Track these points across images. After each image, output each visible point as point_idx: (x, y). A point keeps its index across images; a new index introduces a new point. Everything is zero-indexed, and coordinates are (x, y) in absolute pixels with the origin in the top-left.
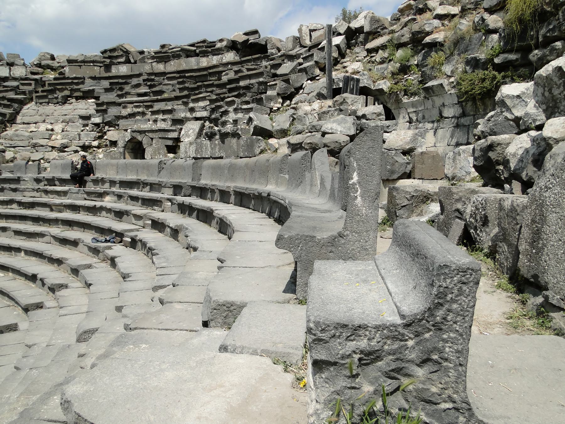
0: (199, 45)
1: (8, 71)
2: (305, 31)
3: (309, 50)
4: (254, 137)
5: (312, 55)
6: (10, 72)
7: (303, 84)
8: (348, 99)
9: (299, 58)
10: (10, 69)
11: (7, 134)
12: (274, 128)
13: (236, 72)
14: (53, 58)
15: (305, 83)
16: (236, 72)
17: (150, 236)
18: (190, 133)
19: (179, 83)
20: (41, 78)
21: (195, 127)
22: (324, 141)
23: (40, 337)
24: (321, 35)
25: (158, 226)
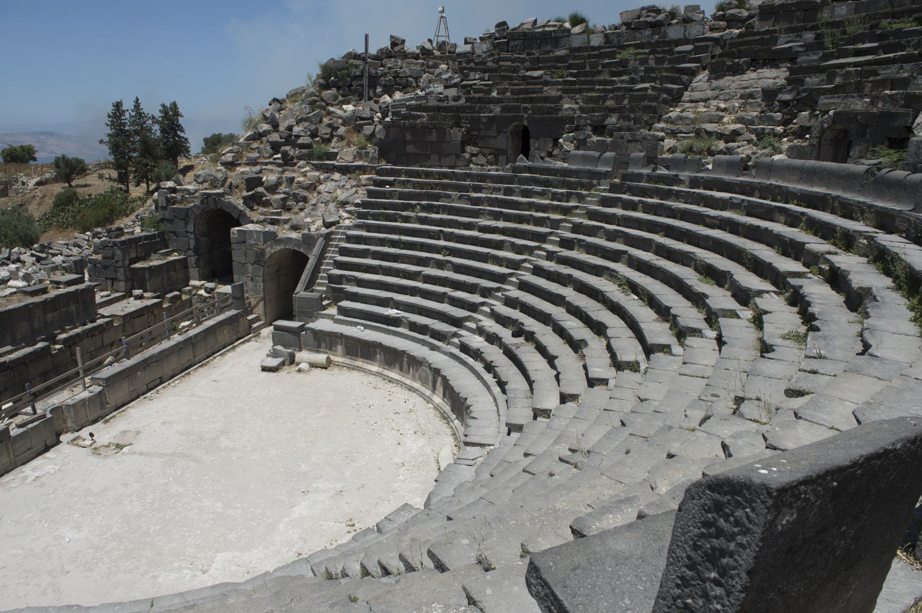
17: (817, 291)
23: (655, 391)
25: (836, 279)
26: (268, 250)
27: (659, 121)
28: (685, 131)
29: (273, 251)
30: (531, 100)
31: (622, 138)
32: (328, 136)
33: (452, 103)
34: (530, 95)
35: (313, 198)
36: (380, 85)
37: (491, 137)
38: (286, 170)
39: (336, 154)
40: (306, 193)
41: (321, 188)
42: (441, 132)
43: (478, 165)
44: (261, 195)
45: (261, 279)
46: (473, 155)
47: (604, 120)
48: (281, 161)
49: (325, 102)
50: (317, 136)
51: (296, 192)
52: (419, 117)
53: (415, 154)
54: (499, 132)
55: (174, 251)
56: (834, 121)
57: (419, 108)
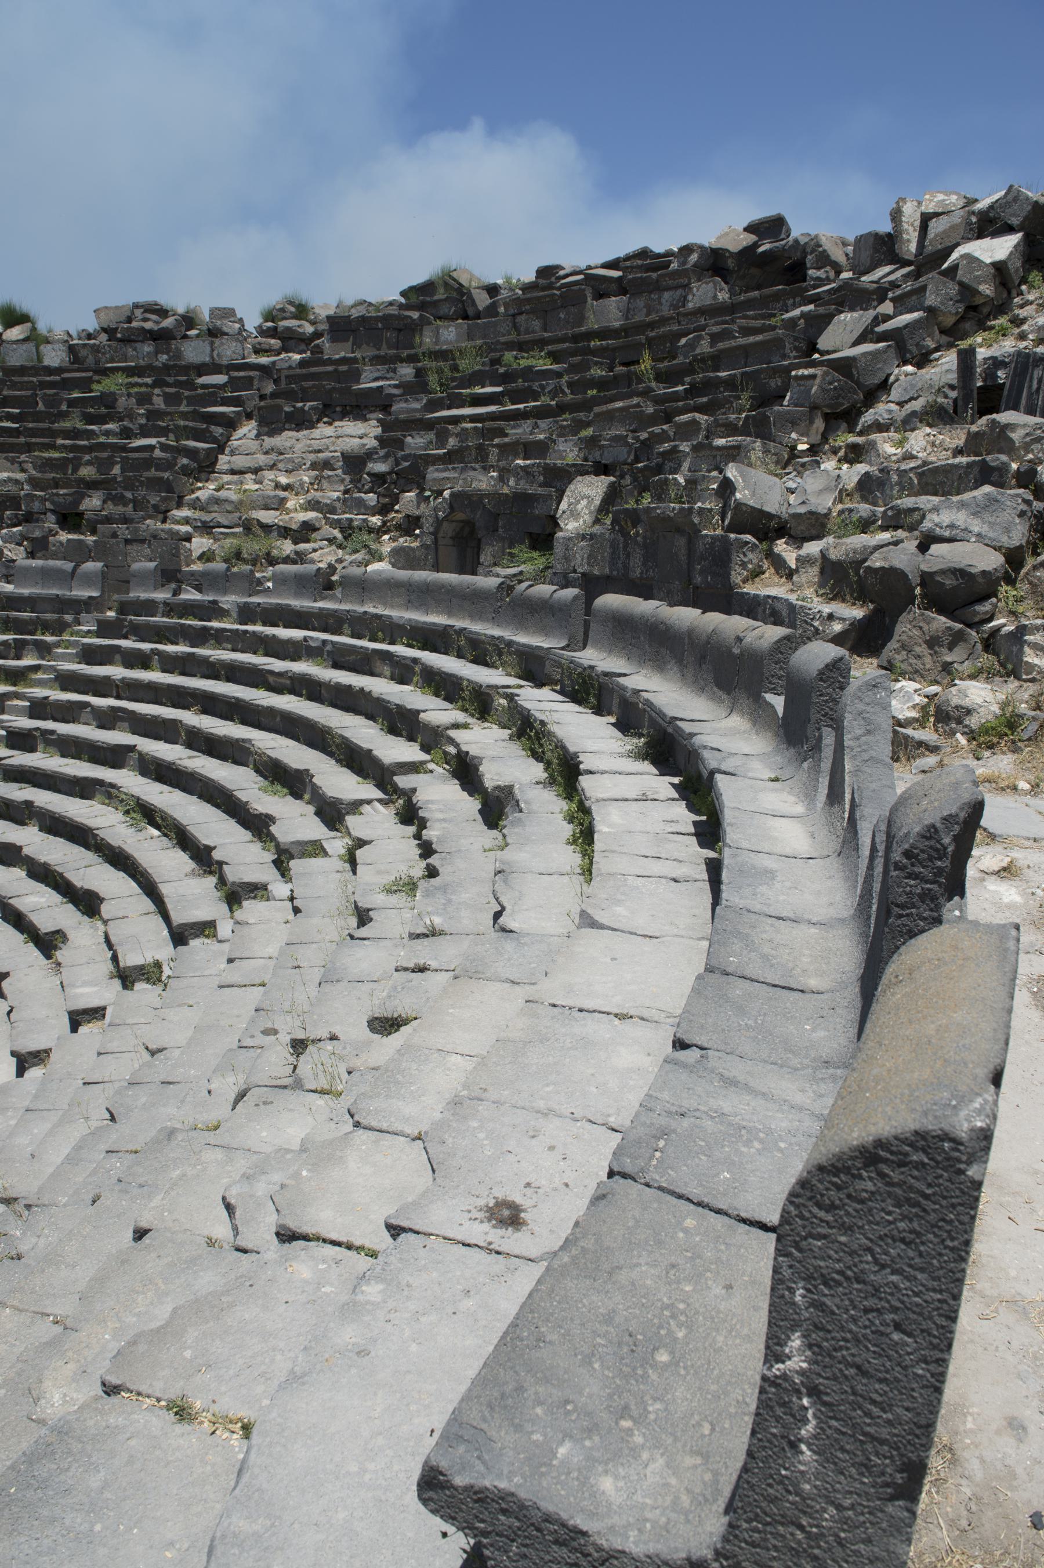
0: (628, 263)
1: (208, 349)
2: (911, 213)
3: (917, 275)
4: (732, 536)
5: (923, 288)
6: (213, 350)
7: (889, 375)
8: (1013, 430)
9: (882, 300)
10: (212, 344)
11: (198, 498)
12: (792, 511)
13: (715, 338)
14: (302, 311)
15: (896, 371)
16: (715, 338)
18: (579, 507)
19: (573, 369)
20: (274, 363)
21: (593, 493)
22: (924, 567)
24: (953, 228)
25: (465, 771)
27: (179, 505)
28: (226, 523)
47: (78, 502)
56: (451, 507)
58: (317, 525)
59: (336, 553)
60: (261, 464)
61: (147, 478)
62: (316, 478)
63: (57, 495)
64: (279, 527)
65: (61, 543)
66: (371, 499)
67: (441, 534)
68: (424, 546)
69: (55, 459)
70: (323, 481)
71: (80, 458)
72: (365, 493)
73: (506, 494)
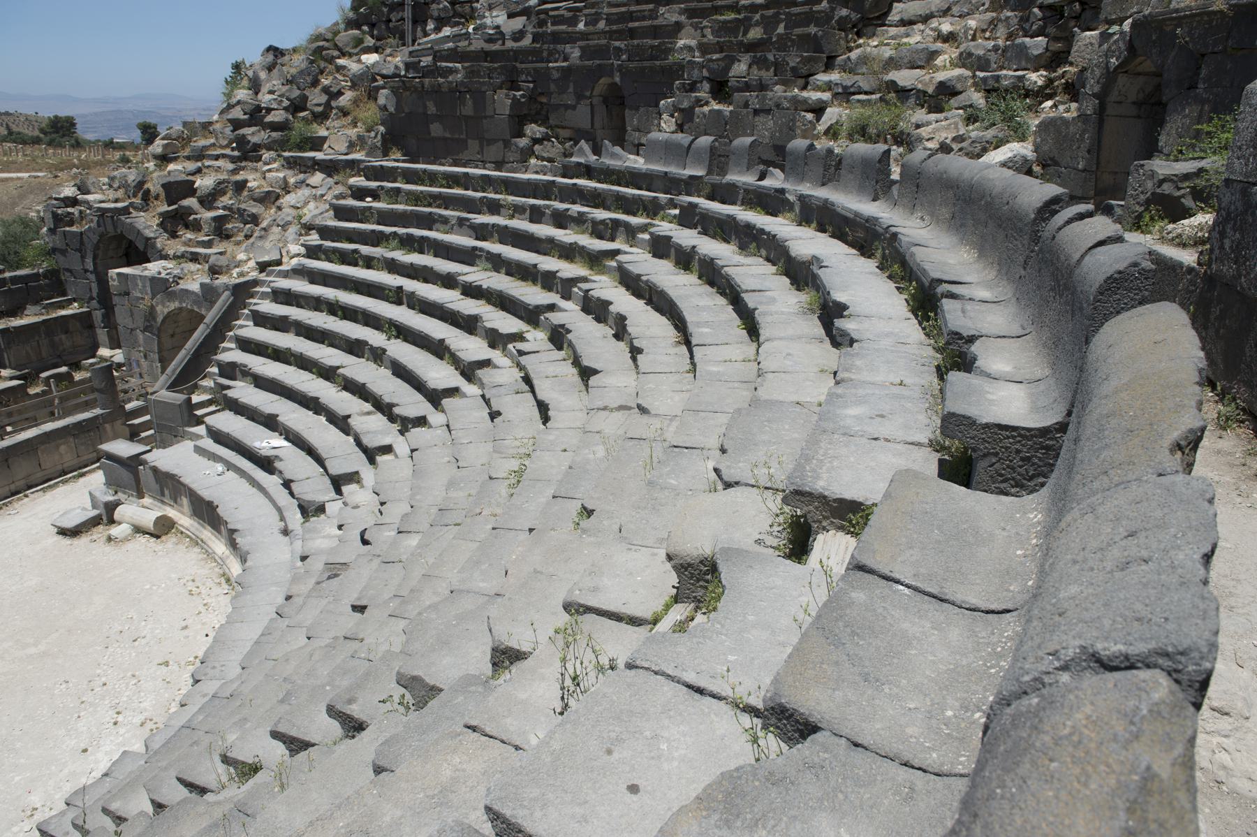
26: (159, 308)
27: (829, 66)
28: (866, 88)
29: (166, 311)
30: (632, 33)
31: (746, 105)
32: (320, 109)
33: (510, 44)
34: (631, 25)
35: (268, 215)
36: (432, 18)
37: (567, 107)
38: (243, 168)
39: (324, 139)
40: (255, 208)
41: (289, 199)
42: (480, 98)
43: (543, 159)
44: (190, 211)
45: (157, 356)
46: (536, 141)
47: (728, 69)
48: (236, 153)
49: (339, 50)
50: (304, 109)
51: (243, 206)
52: (451, 71)
53: (445, 139)
54: (580, 97)
55: (75, 300)
56: (1131, 48)
57: (455, 55)
58: (959, 87)
59: (957, 128)
60: (934, 9)
61: (798, 36)
62: (991, 22)
63: (711, 60)
64: (919, 91)
65: (704, 114)
66: (1036, 46)
67: (1114, 96)
68: (1082, 117)
69: (729, 22)
70: (1000, 25)
71: (750, 19)
72: (1032, 37)
73: (1221, 12)
